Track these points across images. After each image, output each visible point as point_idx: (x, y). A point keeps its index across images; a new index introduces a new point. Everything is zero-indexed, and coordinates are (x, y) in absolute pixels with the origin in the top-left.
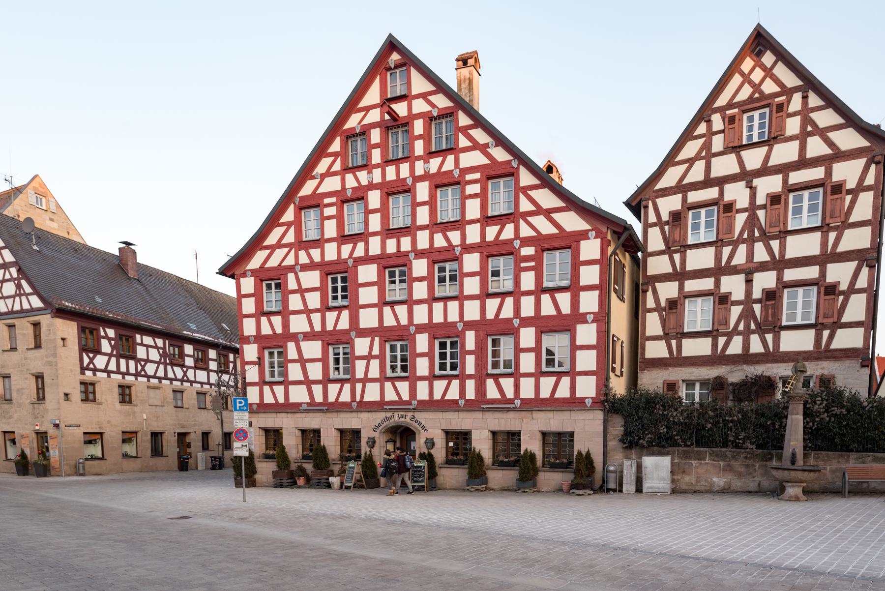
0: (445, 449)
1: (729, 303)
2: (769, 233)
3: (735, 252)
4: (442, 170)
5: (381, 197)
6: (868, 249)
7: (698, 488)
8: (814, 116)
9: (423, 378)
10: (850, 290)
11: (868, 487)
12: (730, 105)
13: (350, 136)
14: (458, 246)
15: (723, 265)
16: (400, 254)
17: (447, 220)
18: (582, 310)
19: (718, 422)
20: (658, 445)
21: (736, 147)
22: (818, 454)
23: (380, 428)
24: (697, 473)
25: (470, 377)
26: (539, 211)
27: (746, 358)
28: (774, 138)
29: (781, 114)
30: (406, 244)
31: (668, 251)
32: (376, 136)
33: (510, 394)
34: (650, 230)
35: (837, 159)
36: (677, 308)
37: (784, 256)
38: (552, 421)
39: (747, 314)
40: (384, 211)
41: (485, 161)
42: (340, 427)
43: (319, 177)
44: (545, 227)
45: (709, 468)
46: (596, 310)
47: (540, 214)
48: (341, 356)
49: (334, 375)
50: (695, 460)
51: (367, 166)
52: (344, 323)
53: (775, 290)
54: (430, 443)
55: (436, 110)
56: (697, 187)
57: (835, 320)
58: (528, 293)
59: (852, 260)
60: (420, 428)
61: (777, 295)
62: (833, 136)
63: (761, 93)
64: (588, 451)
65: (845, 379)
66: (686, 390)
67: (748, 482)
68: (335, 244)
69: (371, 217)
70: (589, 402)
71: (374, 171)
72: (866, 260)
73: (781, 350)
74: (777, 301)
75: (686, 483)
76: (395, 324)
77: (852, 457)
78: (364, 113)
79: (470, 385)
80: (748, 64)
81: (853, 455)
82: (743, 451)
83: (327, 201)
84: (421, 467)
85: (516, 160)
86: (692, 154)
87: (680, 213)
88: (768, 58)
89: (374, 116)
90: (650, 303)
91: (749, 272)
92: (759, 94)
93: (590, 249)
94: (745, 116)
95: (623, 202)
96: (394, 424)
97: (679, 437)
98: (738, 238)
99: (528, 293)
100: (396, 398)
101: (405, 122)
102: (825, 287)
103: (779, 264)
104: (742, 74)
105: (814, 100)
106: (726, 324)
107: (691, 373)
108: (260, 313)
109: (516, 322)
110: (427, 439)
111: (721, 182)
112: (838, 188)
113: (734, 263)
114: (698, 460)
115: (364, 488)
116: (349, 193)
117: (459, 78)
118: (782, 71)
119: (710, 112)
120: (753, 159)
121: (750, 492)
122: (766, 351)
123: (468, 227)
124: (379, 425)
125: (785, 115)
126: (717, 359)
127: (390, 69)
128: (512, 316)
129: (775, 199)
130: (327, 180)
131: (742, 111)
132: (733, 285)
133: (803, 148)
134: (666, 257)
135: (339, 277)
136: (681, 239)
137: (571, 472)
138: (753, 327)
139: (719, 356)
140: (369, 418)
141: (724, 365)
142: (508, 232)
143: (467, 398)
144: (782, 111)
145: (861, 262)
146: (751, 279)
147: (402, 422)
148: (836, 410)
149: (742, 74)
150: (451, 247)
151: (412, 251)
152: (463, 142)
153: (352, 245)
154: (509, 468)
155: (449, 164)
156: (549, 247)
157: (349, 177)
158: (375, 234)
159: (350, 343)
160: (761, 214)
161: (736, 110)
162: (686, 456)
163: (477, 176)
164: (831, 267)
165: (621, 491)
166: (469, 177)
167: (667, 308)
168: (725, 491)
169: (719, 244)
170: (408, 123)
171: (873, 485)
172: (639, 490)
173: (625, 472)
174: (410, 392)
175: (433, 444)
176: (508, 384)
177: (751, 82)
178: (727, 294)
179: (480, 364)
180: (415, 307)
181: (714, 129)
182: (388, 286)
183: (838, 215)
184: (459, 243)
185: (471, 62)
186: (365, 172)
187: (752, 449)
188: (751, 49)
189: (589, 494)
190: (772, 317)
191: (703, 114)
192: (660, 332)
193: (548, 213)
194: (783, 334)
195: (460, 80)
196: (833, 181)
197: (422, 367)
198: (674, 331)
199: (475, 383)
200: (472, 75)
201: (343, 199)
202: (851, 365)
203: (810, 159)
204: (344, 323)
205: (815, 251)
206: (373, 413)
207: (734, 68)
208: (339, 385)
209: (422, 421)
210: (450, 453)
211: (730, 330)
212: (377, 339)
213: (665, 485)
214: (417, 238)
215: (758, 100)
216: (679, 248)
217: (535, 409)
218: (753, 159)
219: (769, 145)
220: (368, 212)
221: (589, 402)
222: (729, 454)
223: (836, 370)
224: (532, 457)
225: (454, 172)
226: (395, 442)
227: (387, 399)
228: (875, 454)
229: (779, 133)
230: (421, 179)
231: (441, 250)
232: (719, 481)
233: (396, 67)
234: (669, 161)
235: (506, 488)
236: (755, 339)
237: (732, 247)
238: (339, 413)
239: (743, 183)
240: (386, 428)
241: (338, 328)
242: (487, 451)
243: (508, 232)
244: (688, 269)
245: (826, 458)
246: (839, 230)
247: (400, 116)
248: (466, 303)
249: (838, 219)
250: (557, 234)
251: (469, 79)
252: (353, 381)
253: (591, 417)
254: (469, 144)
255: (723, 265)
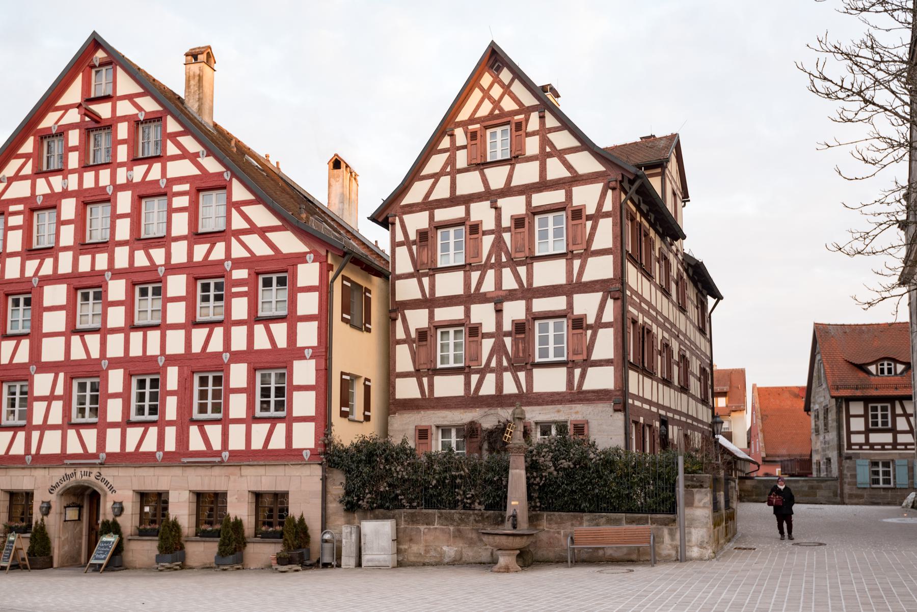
0: (139, 516)
1: (480, 335)
2: (515, 258)
3: (484, 278)
4: (147, 179)
5: (76, 206)
6: (611, 279)
7: (427, 560)
8: (551, 136)
9: (114, 425)
10: (597, 323)
11: (604, 554)
12: (472, 120)
13: (45, 136)
14: (161, 266)
15: (472, 291)
16: (94, 273)
17: (151, 236)
18: (300, 343)
19: (445, 478)
20: (381, 507)
21: (479, 164)
22: (550, 515)
23: (57, 490)
24: (426, 541)
25: (170, 423)
26: (253, 229)
27: (499, 400)
28: (514, 157)
29: (520, 133)
30: (102, 261)
31: (416, 274)
32: (74, 138)
33: (217, 445)
34: (398, 249)
35: (576, 182)
36: (426, 341)
37: (531, 284)
38: (263, 478)
39: (498, 349)
40: (135, 216)
41: (195, 171)
42: (8, 488)
43: (6, 180)
44: (260, 249)
45: (438, 534)
46: (315, 343)
47: (254, 233)
48: (18, 396)
49: (8, 419)
50: (423, 524)
51: (62, 171)
52: (23, 356)
53: (524, 321)
54: (119, 509)
55: (143, 113)
56: (444, 205)
57: (585, 358)
58: (239, 323)
59: (597, 291)
60: (106, 489)
61: (527, 328)
62: (571, 158)
63: (501, 109)
64: (302, 516)
65: (599, 425)
66: (442, 438)
67: (480, 550)
68: (18, 259)
69: (63, 228)
70: (306, 455)
71: (70, 176)
72: (610, 292)
73: (534, 391)
74: (527, 334)
75: (414, 553)
76: (85, 357)
77: (585, 518)
78: (62, 112)
79: (171, 433)
80: (486, 80)
81: (587, 516)
82: (471, 512)
83: (12, 208)
84: (110, 542)
85: (229, 172)
86: (437, 169)
87: (427, 232)
88: (506, 75)
89: (73, 116)
90: (400, 334)
91: (498, 300)
92: (499, 110)
93: (308, 274)
94: (488, 132)
95: (368, 218)
96: (74, 484)
97: (403, 497)
98: (486, 263)
99: (239, 323)
100: (80, 451)
101: (108, 124)
102: (573, 320)
103: (528, 293)
104: (482, 89)
105: (551, 122)
106: (477, 360)
107: (443, 418)
108: (72, 330)
109: (226, 357)
110: (115, 503)
111: (468, 200)
112: (577, 214)
113: (483, 290)
114: (427, 524)
115: (26, 568)
116: (39, 201)
117: (188, 74)
118: (518, 88)
119: (453, 126)
120: (497, 177)
121: (484, 563)
122: (519, 392)
123: (173, 244)
124: (57, 485)
125: (524, 134)
126: (471, 400)
127: (94, 66)
128: (221, 349)
129: (519, 222)
130: (15, 184)
131: (484, 127)
132: (483, 315)
133: (543, 170)
134: (415, 280)
135: (212, 282)
136: (429, 262)
137: (156, 540)
138: (505, 363)
139: (472, 397)
140: (44, 476)
141: (478, 407)
142: (219, 252)
143: (166, 450)
144: (521, 130)
145: (606, 293)
146: (499, 309)
147: (85, 481)
148: (565, 464)
149: (482, 89)
150: (153, 267)
151: (108, 270)
152: (172, 149)
153: (39, 260)
154: (211, 539)
155: (155, 172)
156: (264, 270)
157: (41, 183)
158: (66, 249)
159: (29, 379)
160: (507, 237)
161: (478, 126)
162: (413, 519)
163: (186, 187)
164: (577, 298)
165: (339, 566)
166: (176, 188)
167: (417, 340)
168: (456, 563)
169: (468, 268)
170: (111, 126)
171: (609, 552)
172: (359, 564)
173: (344, 541)
174: (97, 442)
175: (121, 509)
176: (214, 432)
177: (490, 98)
178: (478, 326)
179: (184, 407)
180: (109, 337)
181: (458, 144)
182: (199, 303)
183: (580, 242)
184: (163, 262)
185: (202, 57)
186: (60, 178)
187: (480, 510)
188: (489, 65)
189: (297, 571)
190: (523, 353)
191: (445, 128)
192: (411, 368)
193: (262, 232)
194: (536, 372)
195: (189, 77)
196: (574, 205)
197: (114, 410)
198: (425, 366)
199: (177, 431)
200: (203, 72)
201: (32, 208)
202: (604, 409)
203: (550, 181)
204: (23, 356)
205: (561, 280)
206: (51, 469)
207: (472, 83)
208: (11, 433)
209: (110, 480)
210: (260, 523)
211: (483, 366)
212: (61, 376)
213: (386, 556)
214: (172, 251)
215: (498, 117)
216: (427, 271)
217: (245, 463)
218: (497, 177)
219: (511, 164)
220: (60, 223)
221: (306, 455)
222: (456, 517)
223: (590, 414)
224: (238, 524)
225: (161, 182)
226: (80, 507)
227: (70, 451)
228: (608, 514)
229: (520, 152)
230: (123, 188)
231: (143, 270)
232: (450, 551)
233: (101, 65)
234: (414, 175)
235: (208, 566)
236: (508, 376)
237: (480, 272)
238: (8, 470)
239: (488, 203)
240: (65, 488)
241: (15, 361)
242: (187, 517)
243: (219, 252)
244: (437, 295)
245: (559, 520)
246: (583, 257)
247: (103, 117)
248: (169, 333)
249: (579, 247)
250: (272, 255)
251: (199, 75)
252: (28, 428)
253: (308, 473)
254: (178, 152)
255: (472, 291)
